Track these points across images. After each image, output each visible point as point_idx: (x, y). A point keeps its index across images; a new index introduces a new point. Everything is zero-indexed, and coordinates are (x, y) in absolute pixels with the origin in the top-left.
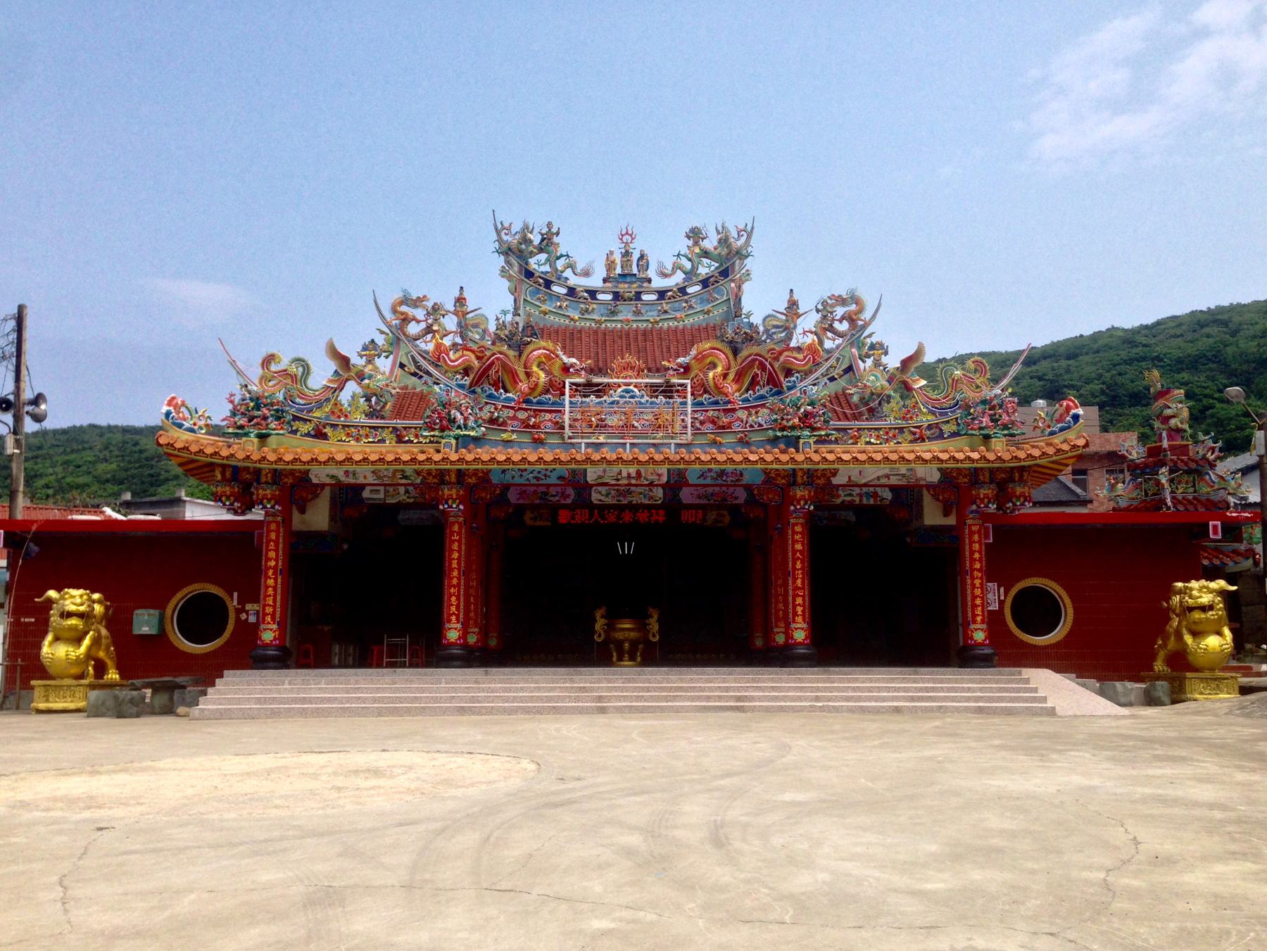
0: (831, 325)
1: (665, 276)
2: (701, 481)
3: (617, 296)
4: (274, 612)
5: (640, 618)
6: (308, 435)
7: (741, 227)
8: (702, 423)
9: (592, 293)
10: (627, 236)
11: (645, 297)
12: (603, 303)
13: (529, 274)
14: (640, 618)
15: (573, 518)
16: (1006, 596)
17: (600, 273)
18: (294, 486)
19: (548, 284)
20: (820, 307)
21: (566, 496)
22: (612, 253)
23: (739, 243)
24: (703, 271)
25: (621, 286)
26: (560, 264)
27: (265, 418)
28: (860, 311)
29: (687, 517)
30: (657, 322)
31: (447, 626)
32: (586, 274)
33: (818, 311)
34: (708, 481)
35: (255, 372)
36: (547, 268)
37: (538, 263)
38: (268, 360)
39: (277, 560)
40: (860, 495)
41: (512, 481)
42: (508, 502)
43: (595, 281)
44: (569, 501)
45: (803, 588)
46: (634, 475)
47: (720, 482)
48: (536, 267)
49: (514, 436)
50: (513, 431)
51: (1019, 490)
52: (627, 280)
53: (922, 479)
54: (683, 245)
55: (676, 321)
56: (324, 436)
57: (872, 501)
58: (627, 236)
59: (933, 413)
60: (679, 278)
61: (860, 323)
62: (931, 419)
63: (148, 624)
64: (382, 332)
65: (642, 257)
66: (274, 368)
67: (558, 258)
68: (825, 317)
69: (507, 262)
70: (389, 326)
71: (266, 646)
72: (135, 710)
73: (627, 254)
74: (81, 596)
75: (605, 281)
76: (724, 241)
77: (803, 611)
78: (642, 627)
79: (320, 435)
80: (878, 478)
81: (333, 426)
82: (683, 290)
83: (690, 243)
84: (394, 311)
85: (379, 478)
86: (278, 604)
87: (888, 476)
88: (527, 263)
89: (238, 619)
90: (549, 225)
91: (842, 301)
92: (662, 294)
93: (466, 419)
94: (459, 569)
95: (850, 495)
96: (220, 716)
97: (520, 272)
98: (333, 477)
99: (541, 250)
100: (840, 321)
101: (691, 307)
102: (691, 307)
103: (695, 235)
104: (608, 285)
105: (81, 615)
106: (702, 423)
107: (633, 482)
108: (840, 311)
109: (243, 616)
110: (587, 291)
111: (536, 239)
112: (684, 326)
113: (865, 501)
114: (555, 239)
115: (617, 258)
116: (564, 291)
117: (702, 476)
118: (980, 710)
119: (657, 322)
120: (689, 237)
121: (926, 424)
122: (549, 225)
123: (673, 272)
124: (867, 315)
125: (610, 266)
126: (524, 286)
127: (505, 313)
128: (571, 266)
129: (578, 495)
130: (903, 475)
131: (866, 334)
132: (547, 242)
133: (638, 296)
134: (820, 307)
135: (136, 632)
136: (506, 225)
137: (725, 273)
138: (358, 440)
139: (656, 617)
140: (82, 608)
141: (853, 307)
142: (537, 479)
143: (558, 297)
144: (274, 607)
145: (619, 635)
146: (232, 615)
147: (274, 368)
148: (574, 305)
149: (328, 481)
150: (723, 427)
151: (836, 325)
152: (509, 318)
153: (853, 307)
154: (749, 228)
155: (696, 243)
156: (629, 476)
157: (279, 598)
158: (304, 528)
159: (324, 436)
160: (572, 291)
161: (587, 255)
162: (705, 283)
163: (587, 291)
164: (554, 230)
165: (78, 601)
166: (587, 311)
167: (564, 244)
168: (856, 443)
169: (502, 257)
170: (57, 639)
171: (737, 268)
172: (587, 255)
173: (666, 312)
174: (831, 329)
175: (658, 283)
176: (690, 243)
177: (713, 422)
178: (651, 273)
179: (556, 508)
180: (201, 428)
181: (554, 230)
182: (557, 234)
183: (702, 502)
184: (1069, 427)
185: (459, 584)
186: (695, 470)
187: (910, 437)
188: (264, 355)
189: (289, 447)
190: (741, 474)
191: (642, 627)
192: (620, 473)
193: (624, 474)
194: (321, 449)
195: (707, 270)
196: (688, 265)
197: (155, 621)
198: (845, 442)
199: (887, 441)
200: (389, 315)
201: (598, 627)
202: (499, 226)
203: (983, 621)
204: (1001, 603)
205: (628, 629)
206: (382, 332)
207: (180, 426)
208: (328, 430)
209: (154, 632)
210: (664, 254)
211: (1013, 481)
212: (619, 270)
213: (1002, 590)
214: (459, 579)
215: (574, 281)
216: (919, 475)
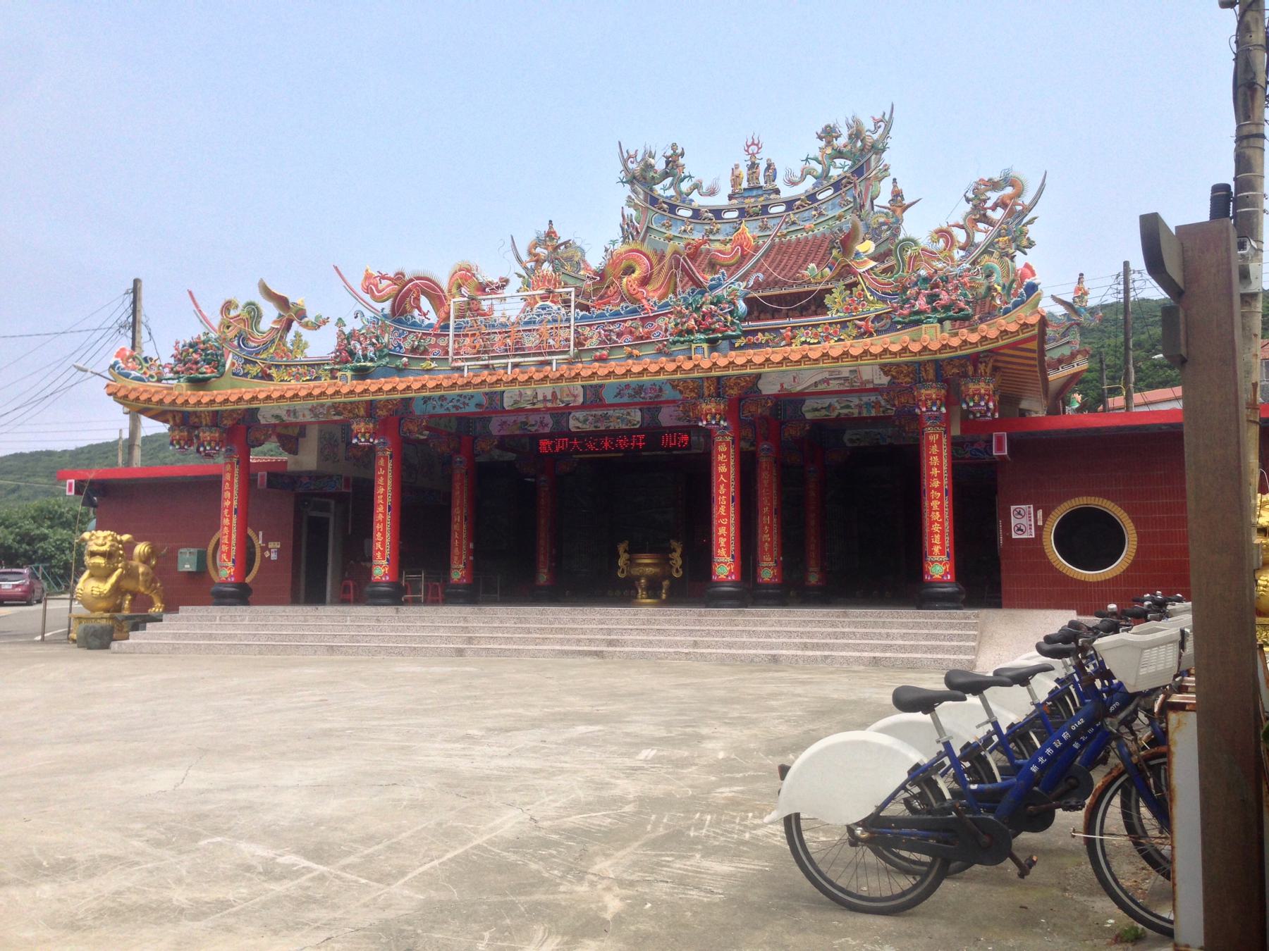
0: (985, 215)
1: (793, 184)
2: (618, 400)
3: (743, 213)
4: (229, 551)
5: (662, 552)
6: (255, 377)
7: (878, 117)
8: (619, 335)
9: (718, 213)
10: (753, 146)
11: (773, 210)
12: (729, 222)
13: (654, 201)
14: (662, 552)
15: (553, 446)
16: (1044, 521)
17: (726, 189)
18: (240, 428)
19: (673, 208)
20: (970, 195)
21: (543, 424)
22: (737, 166)
23: (875, 137)
24: (835, 173)
25: (747, 201)
26: (685, 186)
27: (196, 363)
28: (1019, 194)
29: (666, 441)
30: (785, 236)
31: (929, 558)
32: (712, 192)
33: (968, 200)
34: (626, 400)
35: (216, 320)
36: (671, 192)
37: (663, 190)
38: (227, 306)
39: (231, 500)
40: (860, 406)
41: (432, 412)
42: (490, 434)
43: (721, 200)
44: (547, 430)
45: (728, 516)
46: (549, 397)
47: (637, 400)
48: (661, 192)
49: (433, 365)
50: (432, 360)
51: (972, 387)
52: (754, 195)
53: (868, 382)
54: (815, 147)
55: (822, 234)
56: (269, 377)
57: (873, 414)
58: (753, 146)
59: (884, 301)
60: (810, 182)
61: (1019, 208)
62: (880, 307)
63: (188, 561)
64: (520, 276)
65: (769, 166)
66: (233, 313)
67: (682, 180)
68: (975, 207)
69: (634, 191)
70: (525, 268)
71: (378, 583)
72: (97, 642)
73: (753, 166)
74: (105, 538)
75: (730, 197)
76: (856, 135)
77: (727, 543)
78: (665, 562)
79: (267, 377)
80: (816, 384)
81: (278, 366)
82: (812, 197)
83: (823, 144)
84: (530, 253)
85: (316, 416)
86: (234, 542)
87: (826, 381)
88: (652, 190)
89: (263, 556)
90: (674, 147)
91: (994, 185)
92: (790, 204)
93: (365, 349)
94: (385, 505)
95: (848, 407)
96: (155, 652)
97: (645, 200)
98: (277, 417)
99: (666, 175)
100: (994, 208)
101: (821, 214)
102: (821, 214)
103: (828, 134)
104: (734, 201)
105: (102, 554)
106: (619, 335)
107: (549, 405)
108: (993, 197)
109: (267, 554)
110: (711, 211)
111: (660, 165)
112: (815, 237)
113: (865, 414)
114: (681, 161)
115: (744, 171)
116: (689, 213)
117: (619, 394)
118: (876, 662)
119: (785, 236)
120: (820, 138)
121: (873, 315)
122: (674, 147)
123: (803, 178)
124: (1027, 199)
125: (736, 180)
126: (650, 214)
127: (614, 242)
128: (697, 186)
129: (557, 423)
130: (846, 379)
131: (1025, 221)
132: (673, 162)
133: (764, 210)
134: (970, 195)
135: (180, 570)
136: (632, 153)
137: (858, 172)
138: (298, 379)
139: (679, 551)
140: (106, 548)
141: (1009, 190)
142: (456, 407)
143: (683, 220)
144: (229, 545)
145: (636, 571)
146: (258, 551)
147: (233, 313)
148: (698, 227)
149: (274, 421)
150: (641, 338)
151: (989, 213)
152: (618, 246)
153: (1009, 190)
154: (887, 117)
155: (829, 143)
156: (545, 400)
157: (234, 536)
158: (297, 469)
159: (269, 377)
160: (697, 213)
161: (712, 174)
162: (837, 186)
163: (711, 211)
164: (679, 151)
165: (100, 541)
166: (711, 232)
167: (689, 164)
168: (790, 344)
169: (628, 186)
170: (91, 576)
171: (873, 164)
172: (712, 174)
173: (794, 223)
174: (985, 219)
175: (787, 192)
176: (823, 144)
177: (631, 333)
178: (779, 183)
179: (535, 438)
180: (152, 376)
181: (679, 151)
182: (682, 154)
183: (681, 423)
184: (1023, 302)
185: (384, 520)
186: (611, 385)
187: (854, 333)
188: (222, 303)
189: (232, 391)
190: (661, 390)
191: (665, 562)
192: (536, 396)
193: (540, 397)
194: (263, 389)
195: (840, 171)
196: (819, 168)
197: (195, 558)
198: (778, 345)
199: (827, 338)
200: (525, 257)
201: (621, 562)
202: (625, 155)
203: (942, 552)
204: (1039, 530)
205: (647, 565)
206: (520, 276)
207: (127, 376)
208: (273, 372)
209: (194, 569)
210: (793, 158)
211: (965, 375)
212: (745, 185)
213: (1040, 513)
214: (384, 514)
215: (698, 200)
216: (865, 378)
